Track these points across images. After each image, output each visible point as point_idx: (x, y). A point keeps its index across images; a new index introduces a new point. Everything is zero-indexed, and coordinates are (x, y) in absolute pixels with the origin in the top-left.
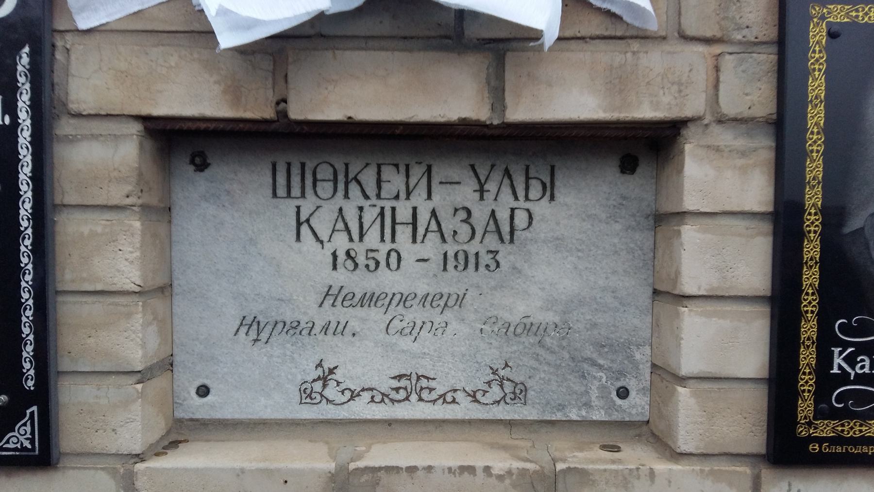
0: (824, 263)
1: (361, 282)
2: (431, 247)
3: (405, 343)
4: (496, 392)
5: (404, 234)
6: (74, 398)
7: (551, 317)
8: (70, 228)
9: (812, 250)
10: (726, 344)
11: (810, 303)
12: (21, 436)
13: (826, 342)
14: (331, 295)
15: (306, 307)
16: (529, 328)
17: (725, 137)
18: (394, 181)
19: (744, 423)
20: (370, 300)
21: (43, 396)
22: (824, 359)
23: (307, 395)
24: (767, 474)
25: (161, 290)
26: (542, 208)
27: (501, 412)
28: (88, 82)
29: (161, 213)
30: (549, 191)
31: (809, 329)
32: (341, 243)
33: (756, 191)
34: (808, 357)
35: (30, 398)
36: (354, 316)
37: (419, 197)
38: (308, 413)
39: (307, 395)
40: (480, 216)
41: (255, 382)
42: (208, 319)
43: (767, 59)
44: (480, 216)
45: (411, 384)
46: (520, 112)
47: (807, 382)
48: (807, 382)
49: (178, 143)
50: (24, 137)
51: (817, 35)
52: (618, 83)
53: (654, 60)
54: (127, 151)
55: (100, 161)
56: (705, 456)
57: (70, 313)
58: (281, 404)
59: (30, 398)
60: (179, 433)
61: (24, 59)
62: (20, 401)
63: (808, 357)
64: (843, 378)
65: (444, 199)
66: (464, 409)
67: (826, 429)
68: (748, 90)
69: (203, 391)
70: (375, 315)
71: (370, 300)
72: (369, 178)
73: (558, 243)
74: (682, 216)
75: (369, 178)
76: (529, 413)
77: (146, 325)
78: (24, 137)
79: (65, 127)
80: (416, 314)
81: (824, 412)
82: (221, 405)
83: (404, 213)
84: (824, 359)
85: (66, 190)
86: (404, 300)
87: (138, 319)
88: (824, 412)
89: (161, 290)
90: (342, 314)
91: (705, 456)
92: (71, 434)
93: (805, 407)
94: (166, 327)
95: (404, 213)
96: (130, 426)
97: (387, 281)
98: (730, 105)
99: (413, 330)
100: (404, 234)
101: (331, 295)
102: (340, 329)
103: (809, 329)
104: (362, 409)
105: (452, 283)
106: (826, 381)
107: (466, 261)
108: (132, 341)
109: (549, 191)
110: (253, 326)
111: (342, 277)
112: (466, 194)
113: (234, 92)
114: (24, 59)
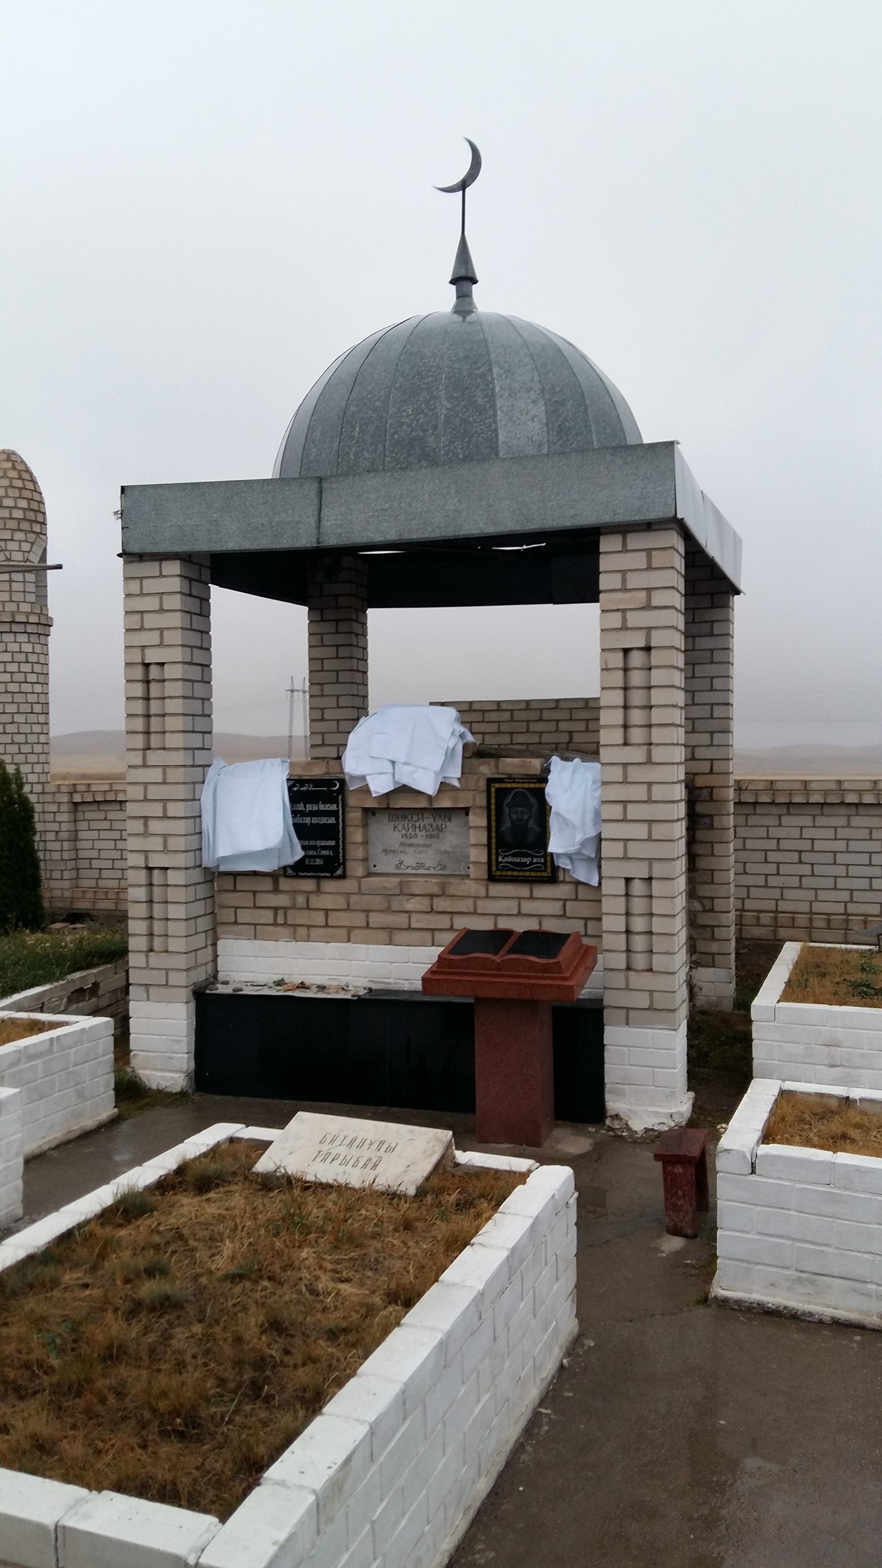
0: (497, 837)
1: (409, 841)
2: (423, 833)
3: (419, 855)
4: (439, 868)
5: (418, 830)
6: (350, 865)
7: (451, 850)
8: (349, 830)
9: (493, 835)
10: (479, 855)
11: (494, 846)
12: (339, 872)
13: (497, 855)
14: (402, 844)
15: (396, 847)
16: (446, 852)
17: (477, 811)
18: (415, 818)
19: (483, 873)
20: (410, 845)
21: (344, 864)
22: (497, 859)
23: (397, 867)
24: (490, 884)
25: (365, 843)
26: (448, 824)
27: (441, 872)
28: (352, 801)
29: (365, 826)
30: (450, 820)
31: (494, 851)
32: (404, 832)
33: (484, 822)
34: (494, 857)
35: (341, 864)
36: (407, 849)
37: (421, 821)
38: (397, 872)
39: (397, 867)
40: (434, 825)
41: (386, 864)
42: (376, 850)
43: (485, 794)
44: (434, 825)
45: (420, 865)
46: (435, 806)
47: (494, 863)
48: (494, 863)
49: (368, 812)
50: (340, 812)
51: (493, 790)
52: (455, 799)
53: (462, 795)
54: (359, 815)
55: (354, 816)
56: (476, 879)
57: (349, 847)
58: (391, 869)
59: (341, 864)
60: (370, 875)
61: (340, 797)
62: (340, 864)
63: (494, 857)
64: (501, 862)
65: (426, 822)
66: (432, 872)
67: (499, 873)
68: (482, 800)
69: (375, 866)
70: (412, 849)
71: (410, 845)
72: (410, 817)
73: (452, 832)
74: (145, 885)
75: (410, 817)
76: (447, 872)
77: (175, 1437)
78: (340, 812)
79: (347, 810)
80: (421, 849)
81: (497, 869)
82: (378, 870)
83: (417, 825)
84: (497, 859)
85: (348, 823)
86: (418, 845)
87: (361, 849)
88: (497, 869)
89: (365, 843)
90: (402, 848)
91: (476, 879)
92: (348, 874)
93: (494, 868)
94: (366, 850)
95: (417, 825)
96: (360, 872)
97: (414, 841)
98: (478, 803)
99: (419, 853)
100: (418, 830)
101: (402, 844)
102: (404, 852)
103: (494, 851)
104: (409, 871)
105: (429, 841)
106: (498, 863)
107: (432, 836)
108: (360, 853)
109: (450, 820)
110: (385, 851)
111: (404, 840)
112: (431, 820)
113: (380, 804)
114: (340, 797)
